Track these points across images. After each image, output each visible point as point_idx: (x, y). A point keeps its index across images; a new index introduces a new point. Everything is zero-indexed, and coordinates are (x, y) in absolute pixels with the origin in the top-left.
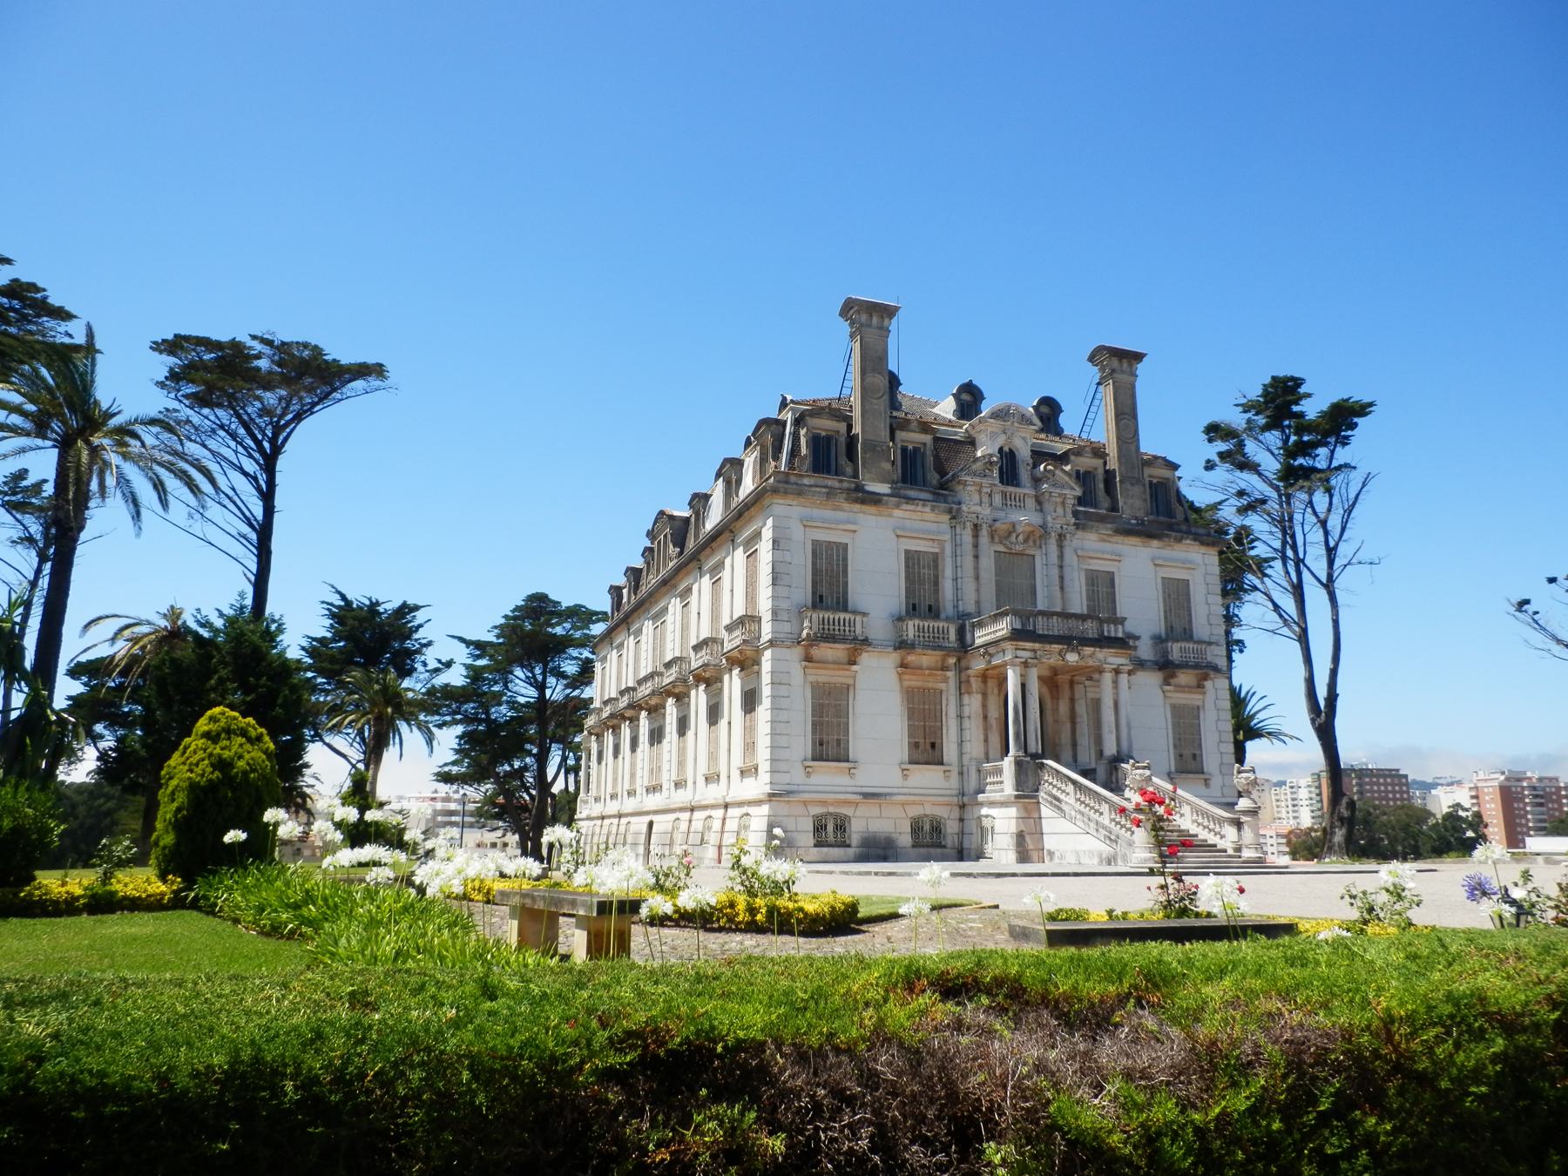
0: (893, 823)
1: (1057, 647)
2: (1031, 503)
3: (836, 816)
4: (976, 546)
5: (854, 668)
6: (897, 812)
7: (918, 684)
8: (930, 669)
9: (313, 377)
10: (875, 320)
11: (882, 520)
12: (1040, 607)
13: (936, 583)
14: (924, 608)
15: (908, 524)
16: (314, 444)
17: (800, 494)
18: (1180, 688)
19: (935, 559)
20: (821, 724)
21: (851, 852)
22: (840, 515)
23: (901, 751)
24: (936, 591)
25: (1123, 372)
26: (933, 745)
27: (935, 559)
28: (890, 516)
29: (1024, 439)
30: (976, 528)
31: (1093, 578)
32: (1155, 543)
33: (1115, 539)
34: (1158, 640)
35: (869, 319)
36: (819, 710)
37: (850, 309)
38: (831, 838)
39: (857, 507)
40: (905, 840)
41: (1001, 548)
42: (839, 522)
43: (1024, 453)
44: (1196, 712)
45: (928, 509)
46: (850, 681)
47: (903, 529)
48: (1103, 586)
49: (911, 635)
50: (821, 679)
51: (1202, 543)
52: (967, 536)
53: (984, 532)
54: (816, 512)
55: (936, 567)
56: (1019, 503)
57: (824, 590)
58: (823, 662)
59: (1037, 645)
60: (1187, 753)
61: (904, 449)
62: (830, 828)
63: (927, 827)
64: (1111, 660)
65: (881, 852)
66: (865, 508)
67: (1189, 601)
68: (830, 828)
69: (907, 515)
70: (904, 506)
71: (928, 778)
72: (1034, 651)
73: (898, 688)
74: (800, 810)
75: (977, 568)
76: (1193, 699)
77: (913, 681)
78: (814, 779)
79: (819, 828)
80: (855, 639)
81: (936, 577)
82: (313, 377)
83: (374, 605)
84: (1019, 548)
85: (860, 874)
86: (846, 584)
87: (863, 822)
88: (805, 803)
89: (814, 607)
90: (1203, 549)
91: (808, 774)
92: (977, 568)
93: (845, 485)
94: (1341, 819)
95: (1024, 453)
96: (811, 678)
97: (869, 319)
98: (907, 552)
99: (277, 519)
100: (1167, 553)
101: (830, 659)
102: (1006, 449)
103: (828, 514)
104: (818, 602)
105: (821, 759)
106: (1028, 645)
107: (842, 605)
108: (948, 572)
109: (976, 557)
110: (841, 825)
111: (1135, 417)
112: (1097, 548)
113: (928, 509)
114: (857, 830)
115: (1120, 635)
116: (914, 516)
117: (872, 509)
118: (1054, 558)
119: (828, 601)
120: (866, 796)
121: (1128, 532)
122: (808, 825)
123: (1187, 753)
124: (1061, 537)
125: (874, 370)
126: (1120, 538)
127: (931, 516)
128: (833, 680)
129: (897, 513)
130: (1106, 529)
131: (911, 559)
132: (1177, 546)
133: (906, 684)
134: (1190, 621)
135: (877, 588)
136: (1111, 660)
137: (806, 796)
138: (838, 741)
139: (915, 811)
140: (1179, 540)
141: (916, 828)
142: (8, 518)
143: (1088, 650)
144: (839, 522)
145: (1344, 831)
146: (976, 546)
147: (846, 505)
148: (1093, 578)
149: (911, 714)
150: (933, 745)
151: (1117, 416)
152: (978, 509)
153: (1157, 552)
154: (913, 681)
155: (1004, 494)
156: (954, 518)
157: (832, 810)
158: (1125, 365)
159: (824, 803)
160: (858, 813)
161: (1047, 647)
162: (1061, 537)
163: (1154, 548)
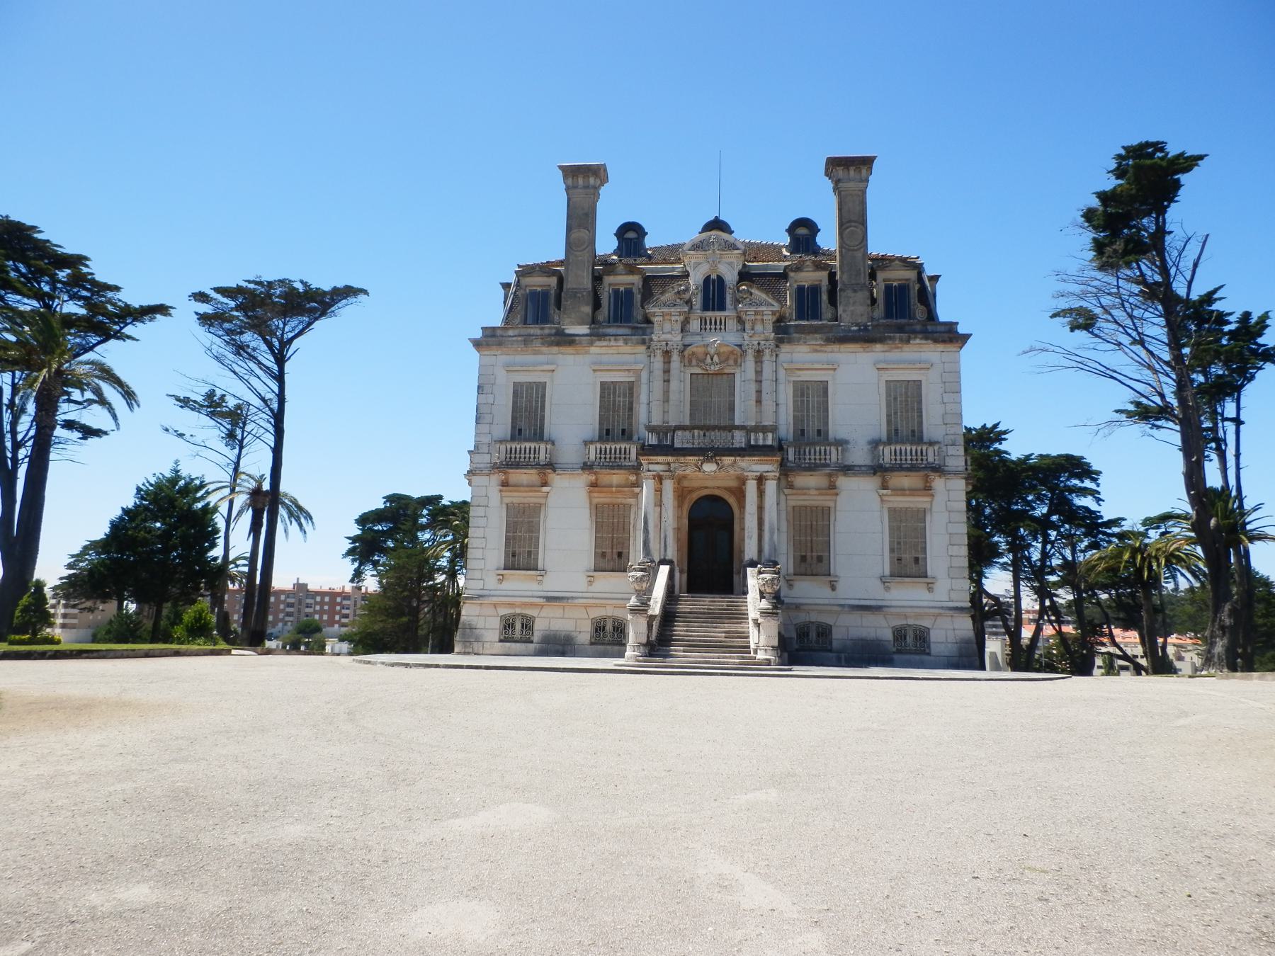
0: (578, 625)
1: (692, 459)
2: (732, 324)
3: (523, 616)
4: (667, 371)
5: (545, 489)
6: (580, 613)
7: (607, 500)
8: (618, 486)
9: (311, 304)
10: (581, 181)
11: (579, 358)
12: (737, 422)
13: (631, 409)
14: (617, 431)
15: (605, 358)
16: (314, 348)
17: (500, 344)
18: (901, 491)
19: (631, 388)
20: (514, 538)
21: (531, 646)
22: (540, 358)
23: (587, 558)
24: (630, 417)
25: (850, 180)
26: (620, 555)
27: (631, 388)
28: (587, 353)
29: (730, 264)
30: (667, 354)
31: (801, 390)
32: (878, 347)
33: (829, 348)
34: (875, 444)
35: (849, 172)
36: (512, 527)
37: (572, 173)
38: (517, 634)
39: (555, 349)
40: (584, 637)
41: (698, 371)
42: (535, 364)
43: (731, 276)
44: (920, 516)
45: (621, 343)
46: (542, 501)
47: (601, 363)
48: (813, 398)
49: (887, 459)
50: (516, 501)
51: (936, 341)
52: (658, 362)
53: (675, 357)
54: (519, 358)
55: (631, 395)
56: (720, 326)
57: (523, 424)
58: (517, 486)
59: (670, 459)
60: (907, 557)
61: (616, 292)
62: (518, 626)
63: (609, 627)
64: (755, 467)
65: (560, 648)
66: (562, 349)
67: (920, 402)
68: (518, 626)
69: (603, 350)
70: (598, 343)
71: (610, 583)
72: (669, 464)
73: (588, 505)
74: (491, 611)
75: (666, 393)
76: (920, 501)
77: (600, 498)
78: (505, 585)
79: (508, 625)
80: (538, 464)
81: (631, 403)
82: (311, 304)
83: (1028, 457)
84: (714, 369)
85: (393, 665)
86: (543, 417)
87: (547, 621)
88: (495, 605)
89: (601, 439)
90: (940, 347)
91: (500, 581)
92: (666, 393)
93: (547, 331)
94: (1223, 628)
95: (731, 276)
96: (507, 500)
97: (849, 172)
98: (602, 383)
99: (288, 407)
100: (895, 355)
101: (525, 482)
102: (714, 276)
103: (530, 358)
104: (517, 434)
105: (513, 568)
106: (660, 459)
107: (539, 436)
108: (643, 398)
109: (667, 381)
110: (528, 625)
111: (863, 222)
112: (806, 358)
113: (621, 343)
114: (540, 627)
115: (769, 442)
116: (610, 351)
117: (569, 349)
118: (751, 374)
119: (526, 433)
120: (549, 599)
121: (845, 338)
122: (496, 623)
123: (907, 557)
124: (759, 353)
125: (579, 226)
126: (836, 347)
127: (627, 349)
128: (526, 501)
129: (593, 350)
130: (817, 340)
131: (607, 389)
132: (906, 348)
133: (596, 501)
134: (920, 423)
135: (573, 416)
136: (755, 467)
137: (495, 600)
138: (530, 552)
139: (597, 613)
140: (908, 341)
141: (599, 628)
142: (213, 423)
143: (728, 460)
144: (542, 364)
145: (1225, 641)
146: (667, 371)
147: (545, 349)
148: (801, 390)
149: (599, 527)
150: (620, 555)
151: (841, 225)
152: (668, 336)
153: (881, 356)
154: (600, 498)
155: (703, 321)
156: (649, 348)
157: (518, 611)
158: (852, 172)
159: (511, 605)
160: (543, 614)
161: (682, 459)
162: (759, 353)
163: (878, 352)
